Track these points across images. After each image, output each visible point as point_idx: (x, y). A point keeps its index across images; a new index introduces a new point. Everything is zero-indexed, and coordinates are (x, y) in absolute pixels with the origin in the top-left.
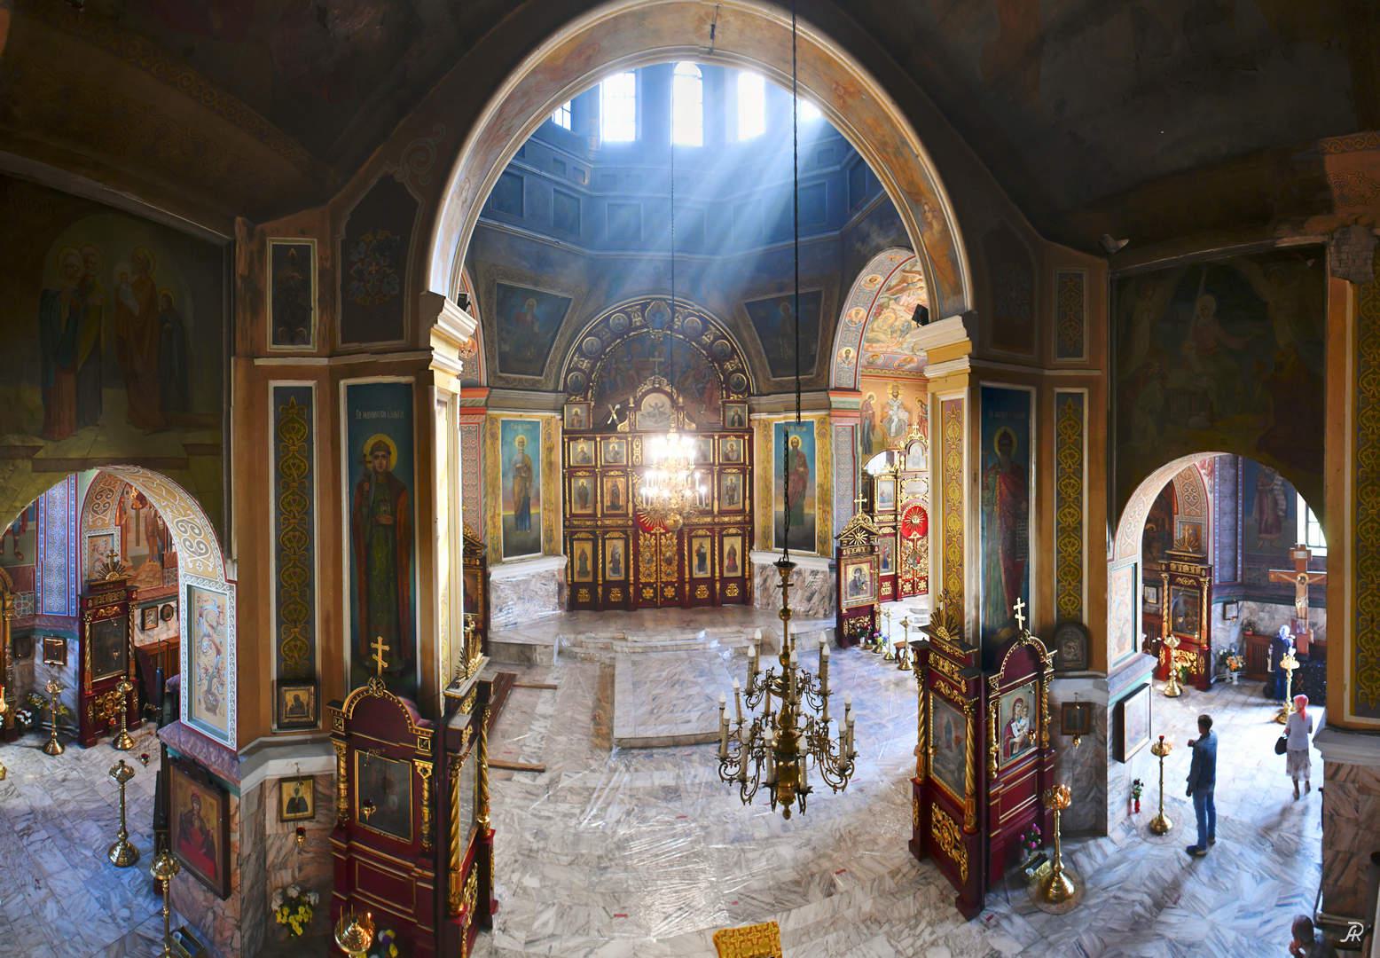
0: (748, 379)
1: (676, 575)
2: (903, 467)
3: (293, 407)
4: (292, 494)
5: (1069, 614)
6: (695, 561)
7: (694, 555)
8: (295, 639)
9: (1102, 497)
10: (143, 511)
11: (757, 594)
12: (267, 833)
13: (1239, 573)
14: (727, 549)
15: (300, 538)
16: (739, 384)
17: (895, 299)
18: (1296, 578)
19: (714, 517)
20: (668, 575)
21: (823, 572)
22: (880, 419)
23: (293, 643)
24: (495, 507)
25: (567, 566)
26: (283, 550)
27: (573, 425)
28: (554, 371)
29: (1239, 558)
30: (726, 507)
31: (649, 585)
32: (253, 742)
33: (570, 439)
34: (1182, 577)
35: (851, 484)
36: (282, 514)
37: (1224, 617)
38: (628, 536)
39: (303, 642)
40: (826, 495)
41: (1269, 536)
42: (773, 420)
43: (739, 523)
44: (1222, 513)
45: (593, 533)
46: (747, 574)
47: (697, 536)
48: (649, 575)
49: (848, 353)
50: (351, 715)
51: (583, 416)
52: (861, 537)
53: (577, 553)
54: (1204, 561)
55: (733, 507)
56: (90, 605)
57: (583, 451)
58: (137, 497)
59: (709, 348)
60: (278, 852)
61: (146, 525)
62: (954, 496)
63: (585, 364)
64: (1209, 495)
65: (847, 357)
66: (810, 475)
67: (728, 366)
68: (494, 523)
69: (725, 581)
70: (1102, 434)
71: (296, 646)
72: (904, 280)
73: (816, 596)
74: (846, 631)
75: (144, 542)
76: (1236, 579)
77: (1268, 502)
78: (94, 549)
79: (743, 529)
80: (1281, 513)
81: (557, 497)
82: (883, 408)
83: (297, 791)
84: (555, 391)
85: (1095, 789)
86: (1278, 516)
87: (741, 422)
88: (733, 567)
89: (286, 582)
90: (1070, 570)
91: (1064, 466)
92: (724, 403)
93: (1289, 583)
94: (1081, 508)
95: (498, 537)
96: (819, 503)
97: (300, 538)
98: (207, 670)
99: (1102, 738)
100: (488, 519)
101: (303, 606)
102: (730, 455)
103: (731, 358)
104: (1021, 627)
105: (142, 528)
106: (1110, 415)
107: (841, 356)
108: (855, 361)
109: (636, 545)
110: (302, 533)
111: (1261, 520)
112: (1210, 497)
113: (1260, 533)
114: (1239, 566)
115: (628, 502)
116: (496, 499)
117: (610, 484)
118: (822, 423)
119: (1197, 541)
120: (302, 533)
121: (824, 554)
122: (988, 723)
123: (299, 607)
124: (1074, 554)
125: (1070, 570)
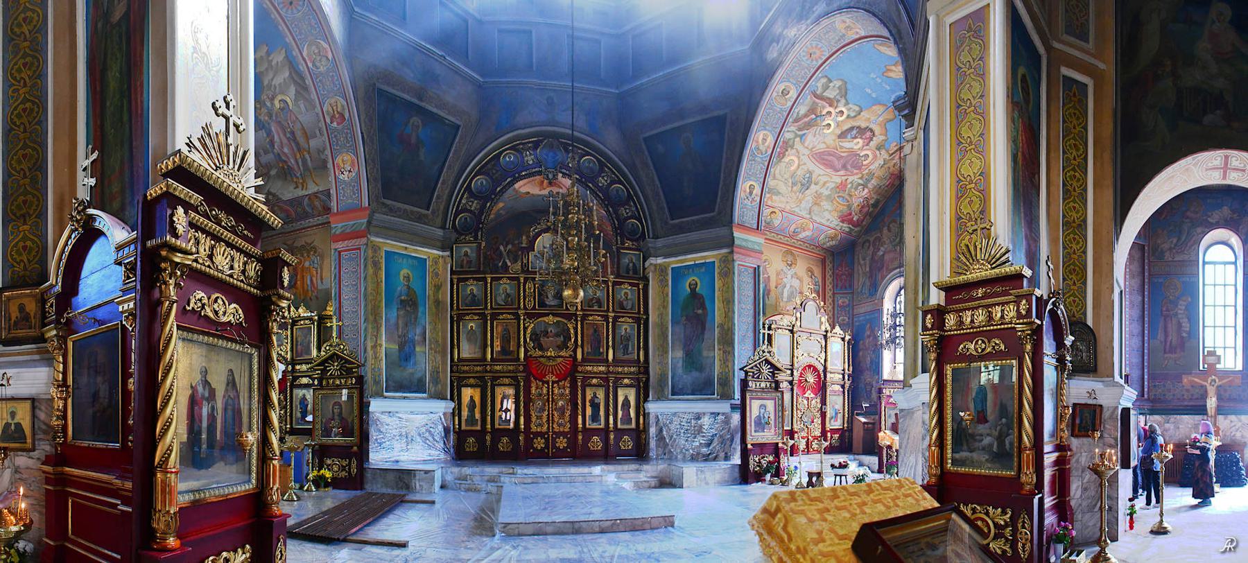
1: (568, 425)
2: (798, 323)
4: (23, 57)
6: (589, 411)
7: (588, 404)
8: (25, 238)
9: (1109, 195)
11: (653, 444)
13: (1146, 390)
14: (621, 399)
15: (32, 110)
16: (634, 231)
17: (801, 137)
18: (1207, 381)
19: (608, 366)
20: (559, 425)
21: (723, 414)
23: (21, 244)
25: (453, 409)
27: (462, 267)
28: (442, 207)
30: (620, 356)
31: (541, 434)
33: (459, 280)
35: (751, 326)
36: (10, 87)
38: (519, 382)
40: (727, 334)
41: (1173, 356)
42: (669, 263)
44: (1132, 335)
45: (482, 378)
46: (641, 426)
47: (591, 385)
48: (541, 425)
51: (473, 255)
53: (466, 400)
57: (472, 293)
59: (605, 191)
63: (475, 205)
65: (751, 193)
66: (709, 318)
68: (375, 353)
69: (620, 433)
70: (1108, 129)
72: (812, 110)
74: (751, 467)
76: (1143, 396)
77: (1172, 327)
79: (638, 380)
80: (1184, 335)
81: (445, 338)
82: (778, 274)
84: (443, 227)
86: (1183, 337)
87: (636, 271)
88: (627, 419)
89: (15, 169)
91: (1069, 155)
92: (618, 249)
93: (1202, 386)
95: (380, 369)
96: (719, 343)
97: (32, 110)
100: (369, 348)
102: (625, 303)
103: (627, 203)
110: (34, 103)
111: (1166, 341)
113: (1165, 353)
114: (1146, 383)
115: (519, 346)
116: (378, 329)
117: (500, 329)
118: (724, 261)
120: (34, 103)
121: (726, 396)
123: (29, 197)
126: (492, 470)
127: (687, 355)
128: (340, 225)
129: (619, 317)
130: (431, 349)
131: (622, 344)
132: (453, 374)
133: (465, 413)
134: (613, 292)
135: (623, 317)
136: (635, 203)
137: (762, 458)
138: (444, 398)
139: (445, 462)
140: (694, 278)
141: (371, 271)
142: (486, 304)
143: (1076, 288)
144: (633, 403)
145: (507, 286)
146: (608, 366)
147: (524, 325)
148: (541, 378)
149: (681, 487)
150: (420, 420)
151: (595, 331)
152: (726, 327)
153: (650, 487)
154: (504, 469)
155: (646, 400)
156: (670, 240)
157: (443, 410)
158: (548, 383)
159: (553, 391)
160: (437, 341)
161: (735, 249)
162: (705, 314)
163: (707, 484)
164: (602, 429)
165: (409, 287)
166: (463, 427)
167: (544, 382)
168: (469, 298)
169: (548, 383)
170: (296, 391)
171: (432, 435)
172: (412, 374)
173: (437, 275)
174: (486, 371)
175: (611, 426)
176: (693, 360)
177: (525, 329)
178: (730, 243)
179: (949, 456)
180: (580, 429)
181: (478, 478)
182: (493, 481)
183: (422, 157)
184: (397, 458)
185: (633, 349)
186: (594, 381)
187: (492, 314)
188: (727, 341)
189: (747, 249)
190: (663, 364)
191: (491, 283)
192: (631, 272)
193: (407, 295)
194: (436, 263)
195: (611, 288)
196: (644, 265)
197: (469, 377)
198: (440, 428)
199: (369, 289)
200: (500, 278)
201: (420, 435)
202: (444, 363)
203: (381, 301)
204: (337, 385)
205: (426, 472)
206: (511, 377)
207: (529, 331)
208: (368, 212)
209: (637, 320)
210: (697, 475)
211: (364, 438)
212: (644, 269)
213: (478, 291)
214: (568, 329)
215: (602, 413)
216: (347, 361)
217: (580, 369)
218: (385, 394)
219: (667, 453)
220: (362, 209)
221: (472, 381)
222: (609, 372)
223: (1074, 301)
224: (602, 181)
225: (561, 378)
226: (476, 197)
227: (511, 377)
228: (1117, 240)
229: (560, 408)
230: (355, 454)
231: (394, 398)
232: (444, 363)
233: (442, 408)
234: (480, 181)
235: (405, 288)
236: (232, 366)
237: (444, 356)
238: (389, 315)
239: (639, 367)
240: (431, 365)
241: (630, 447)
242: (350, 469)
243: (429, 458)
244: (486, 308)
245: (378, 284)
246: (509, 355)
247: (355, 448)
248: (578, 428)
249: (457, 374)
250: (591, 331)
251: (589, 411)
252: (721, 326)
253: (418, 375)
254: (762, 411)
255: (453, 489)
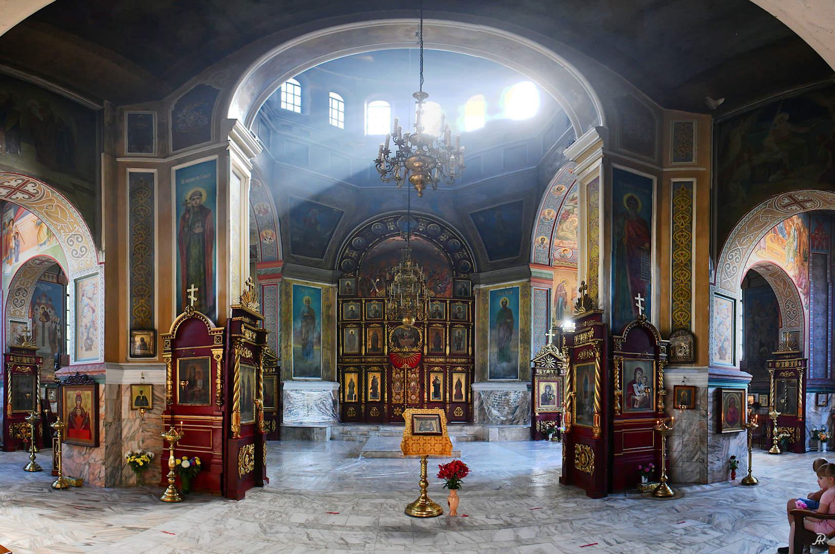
0: (472, 264)
3: (141, 181)
5: (681, 324)
6: (432, 389)
8: (142, 306)
9: (706, 242)
10: (47, 324)
12: (123, 418)
14: (455, 381)
15: (145, 248)
22: (571, 297)
24: (287, 340)
25: (339, 388)
26: (134, 254)
27: (345, 293)
28: (332, 256)
29: (829, 361)
30: (455, 351)
32: (112, 356)
34: (784, 371)
37: (817, 404)
38: (384, 369)
39: (147, 309)
43: (464, 363)
46: (469, 400)
49: (543, 240)
50: (175, 335)
52: (551, 361)
53: (347, 382)
54: (801, 354)
55: (459, 352)
56: (11, 359)
57: (352, 310)
58: (43, 314)
59: (445, 244)
60: (129, 430)
61: (49, 333)
62: (593, 235)
63: (354, 254)
64: (805, 309)
65: (542, 243)
66: (515, 325)
67: (457, 256)
68: (287, 351)
70: (706, 203)
71: (142, 310)
73: (518, 410)
74: (538, 428)
75: (47, 344)
78: (14, 330)
79: (467, 368)
83: (141, 392)
84: (333, 269)
85: (699, 453)
87: (466, 292)
88: (459, 395)
90: (681, 293)
91: (678, 224)
94: (691, 250)
98: (86, 326)
99: (704, 413)
101: (147, 287)
102: (458, 314)
104: (640, 314)
105: (46, 335)
106: (712, 192)
107: (538, 242)
108: (548, 246)
109: (390, 376)
112: (806, 312)
116: (289, 334)
117: (371, 334)
119: (795, 343)
121: (524, 379)
122: (613, 374)
123: (144, 287)
124: (686, 282)
125: (681, 293)
126: (363, 428)
127: (500, 351)
128: (264, 270)
129: (455, 324)
130: (324, 347)
131: (456, 342)
132: (339, 364)
133: (347, 391)
134: (450, 308)
135: (457, 324)
136: (466, 250)
137: (547, 423)
138: (331, 380)
139: (334, 423)
140: (507, 299)
141: (284, 298)
142: (362, 317)
143: (683, 305)
144: (379, 381)
145: (376, 306)
146: (446, 358)
147: (388, 330)
148: (399, 366)
149: (488, 441)
150: (316, 395)
151: (437, 334)
152: (526, 331)
153: (467, 441)
154: (373, 428)
155: (473, 382)
156: (489, 273)
157: (332, 389)
158: (404, 370)
159: (407, 376)
160: (328, 342)
161: (531, 279)
162: (512, 322)
163: (506, 439)
164: (441, 402)
165: (309, 307)
166: (346, 400)
167: (401, 370)
168: (350, 313)
169: (404, 370)
170: (346, 375)
171: (325, 405)
172: (311, 364)
173: (328, 299)
174: (362, 362)
175: (448, 400)
176: (504, 355)
177: (388, 333)
178: (529, 275)
179: (575, 417)
180: (426, 402)
181: (355, 433)
182: (364, 435)
183: (319, 229)
184: (302, 421)
185: (464, 346)
186: (436, 369)
187: (366, 324)
188: (526, 340)
189: (541, 278)
190: (484, 356)
191: (365, 303)
192: (463, 294)
193: (308, 313)
194: (328, 291)
195: (448, 305)
196: (472, 288)
197: (350, 366)
198: (330, 400)
199: (283, 308)
200: (372, 300)
201: (316, 406)
202: (333, 358)
203: (290, 317)
204: (548, 374)
205: (321, 428)
206: (379, 366)
207: (391, 335)
208: (282, 263)
209: (467, 327)
210: (499, 433)
211: (280, 407)
212: (472, 291)
213: (356, 308)
214: (418, 333)
215: (441, 391)
216: (269, 357)
217: (426, 360)
218: (294, 378)
219: (485, 419)
220: (277, 261)
221: (352, 368)
222: (447, 362)
223: (681, 315)
224: (442, 238)
225: (413, 366)
226: (355, 250)
227: (379, 366)
228: (715, 268)
229: (413, 387)
230: (274, 417)
231: (299, 381)
232: (333, 358)
233: (332, 387)
234: (357, 240)
235: (307, 308)
236: (722, 362)
237: (333, 352)
238: (297, 325)
239: (468, 359)
240: (324, 358)
241: (461, 415)
242: (271, 427)
243: (323, 421)
244: (361, 320)
245: (289, 306)
246: (377, 351)
247: (275, 414)
248: (424, 401)
249: (342, 364)
250: (434, 334)
251: (432, 389)
252: (522, 330)
253: (316, 365)
254: (548, 390)
255: (338, 440)
